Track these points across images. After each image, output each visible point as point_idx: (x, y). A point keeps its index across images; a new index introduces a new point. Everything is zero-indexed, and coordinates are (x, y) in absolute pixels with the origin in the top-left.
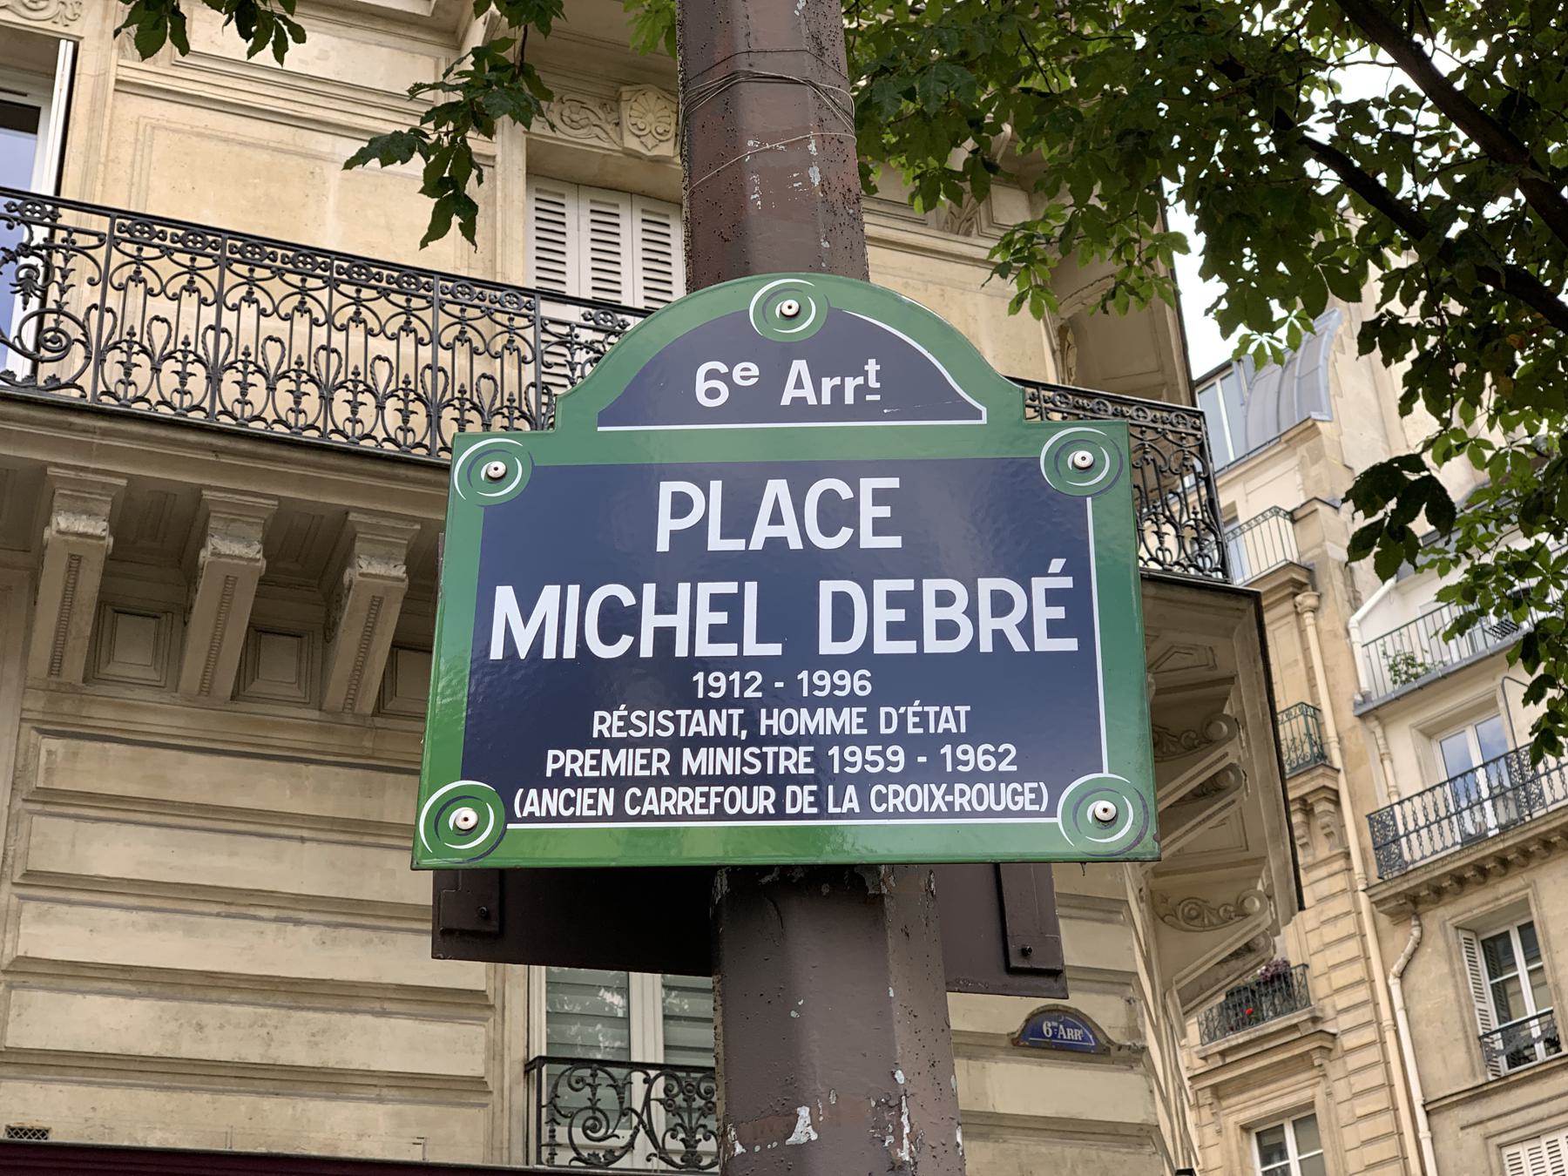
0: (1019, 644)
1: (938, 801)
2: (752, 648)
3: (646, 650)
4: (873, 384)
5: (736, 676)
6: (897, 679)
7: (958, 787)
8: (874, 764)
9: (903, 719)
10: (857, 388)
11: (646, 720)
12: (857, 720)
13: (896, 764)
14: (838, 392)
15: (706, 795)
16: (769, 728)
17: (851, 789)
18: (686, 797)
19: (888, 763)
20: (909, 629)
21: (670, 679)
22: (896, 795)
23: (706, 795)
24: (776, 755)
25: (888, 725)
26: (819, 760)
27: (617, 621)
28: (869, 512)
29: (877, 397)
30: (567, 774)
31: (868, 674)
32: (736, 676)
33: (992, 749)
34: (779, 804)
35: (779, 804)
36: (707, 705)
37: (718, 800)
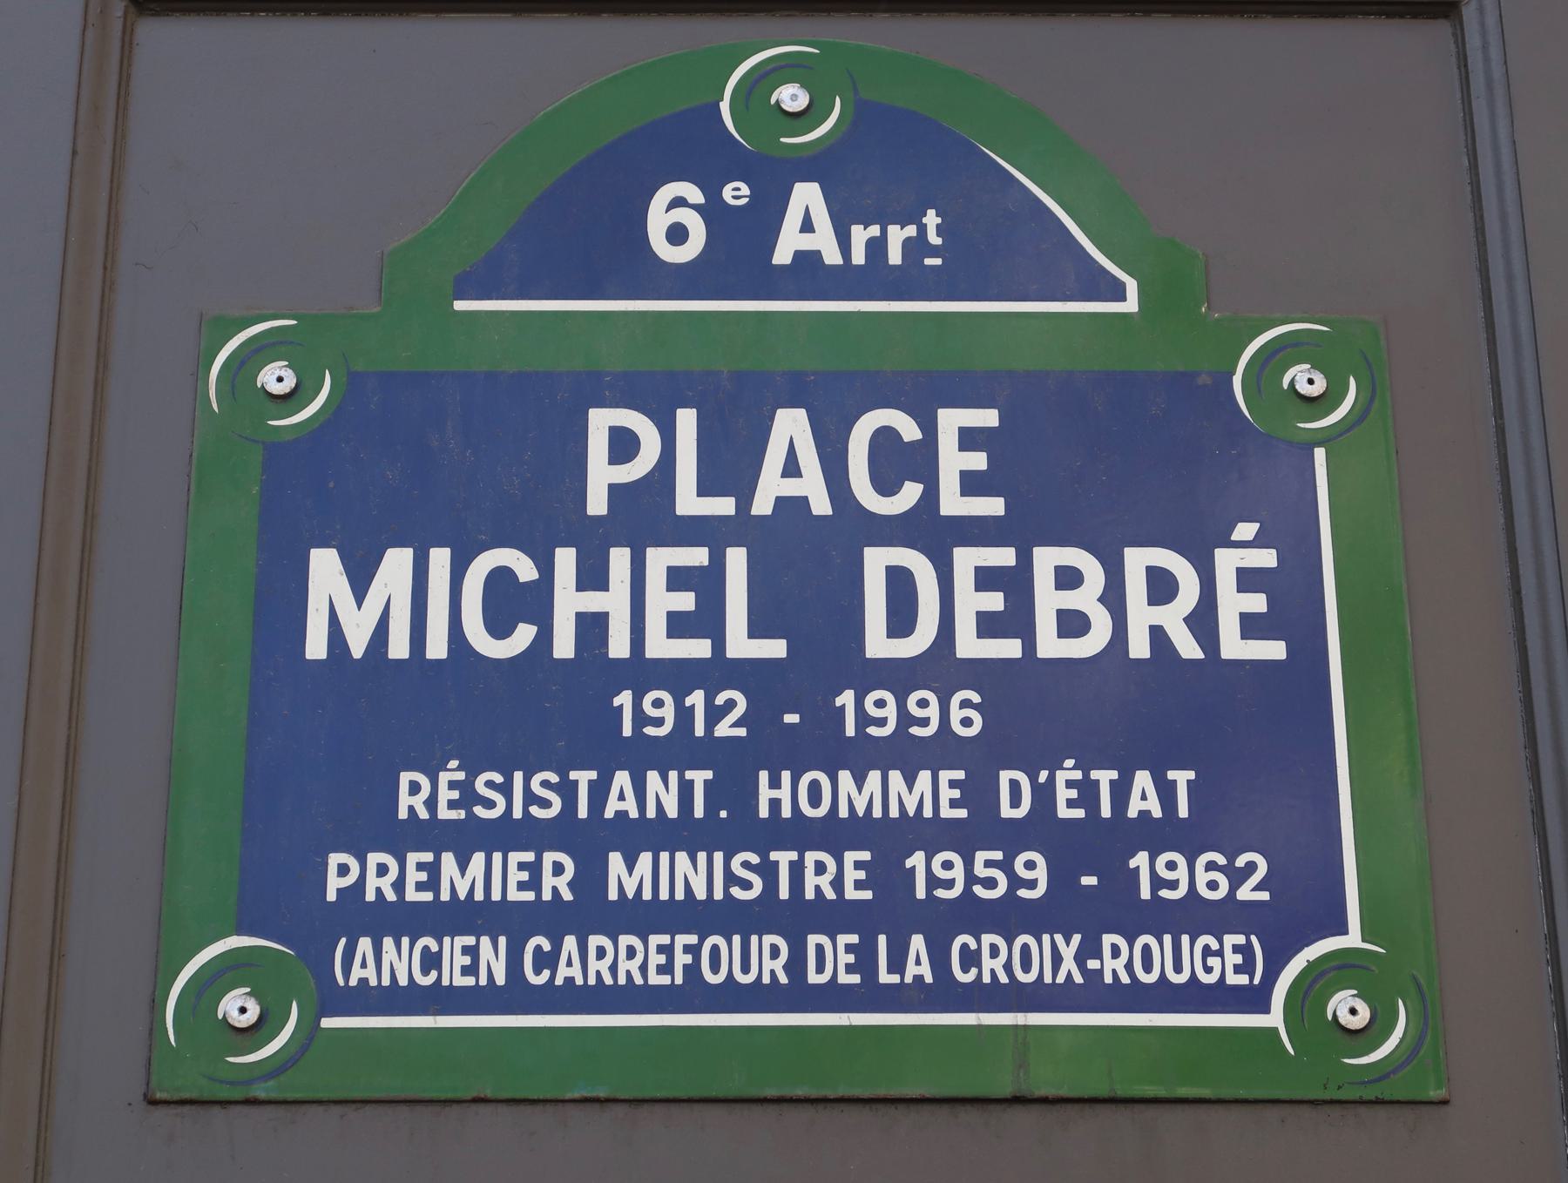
0: (1188, 648)
1: (1069, 964)
2: (740, 644)
3: (564, 646)
4: (934, 239)
5: (697, 699)
6: (1035, 710)
7: (1108, 940)
8: (990, 883)
9: (1044, 795)
10: (907, 243)
11: (506, 789)
12: (947, 794)
13: (1032, 884)
14: (877, 248)
15: (667, 950)
16: (775, 804)
17: (918, 943)
18: (631, 953)
19: (1015, 882)
20: (1015, 619)
21: (558, 709)
22: (994, 951)
23: (667, 950)
24: (797, 869)
25: (1015, 802)
26: (887, 876)
27: (510, 602)
28: (953, 462)
29: (938, 261)
30: (370, 896)
31: (976, 698)
32: (697, 699)
33: (1221, 860)
34: (796, 965)
35: (796, 965)
36: (644, 756)
37: (688, 959)
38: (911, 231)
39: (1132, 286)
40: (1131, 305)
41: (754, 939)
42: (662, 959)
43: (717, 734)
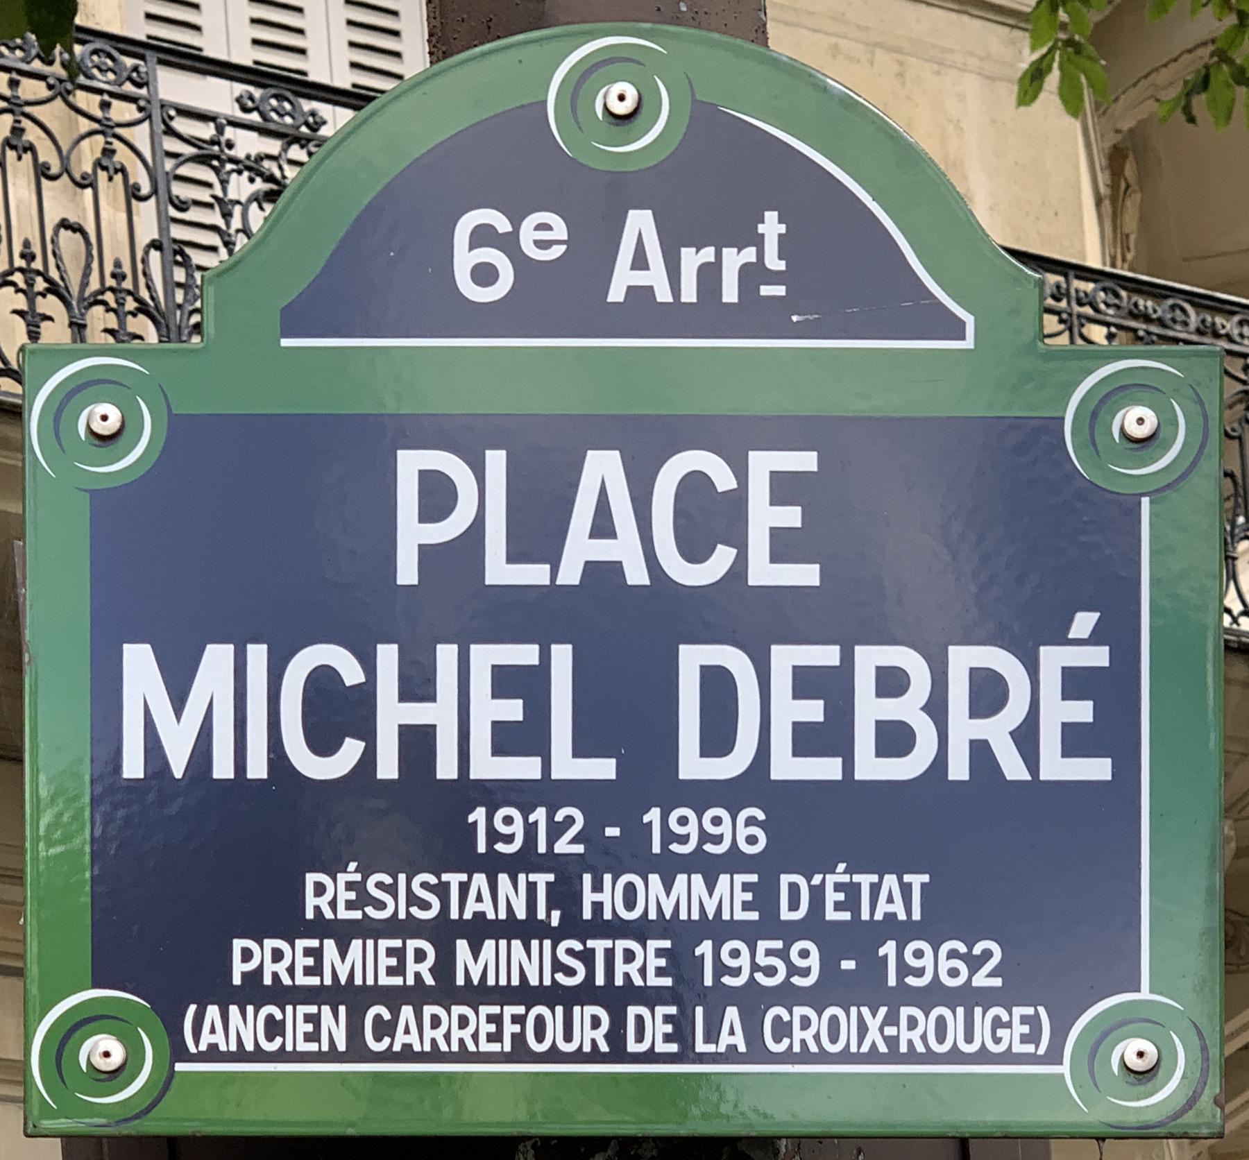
1: (873, 1035)
2: (568, 766)
4: (775, 263)
6: (814, 826)
7: (905, 1012)
8: (770, 971)
9: (817, 894)
10: (745, 270)
13: (805, 972)
14: (710, 275)
15: (496, 1019)
17: (732, 1014)
18: (463, 1022)
23: (496, 1019)
25: (794, 906)
26: (680, 962)
27: (337, 712)
29: (780, 291)
30: (268, 981)
33: (962, 948)
37: (517, 1028)
38: (750, 254)
39: (969, 319)
40: (969, 343)
41: (577, 1009)
42: (492, 1028)
43: (556, 851)
